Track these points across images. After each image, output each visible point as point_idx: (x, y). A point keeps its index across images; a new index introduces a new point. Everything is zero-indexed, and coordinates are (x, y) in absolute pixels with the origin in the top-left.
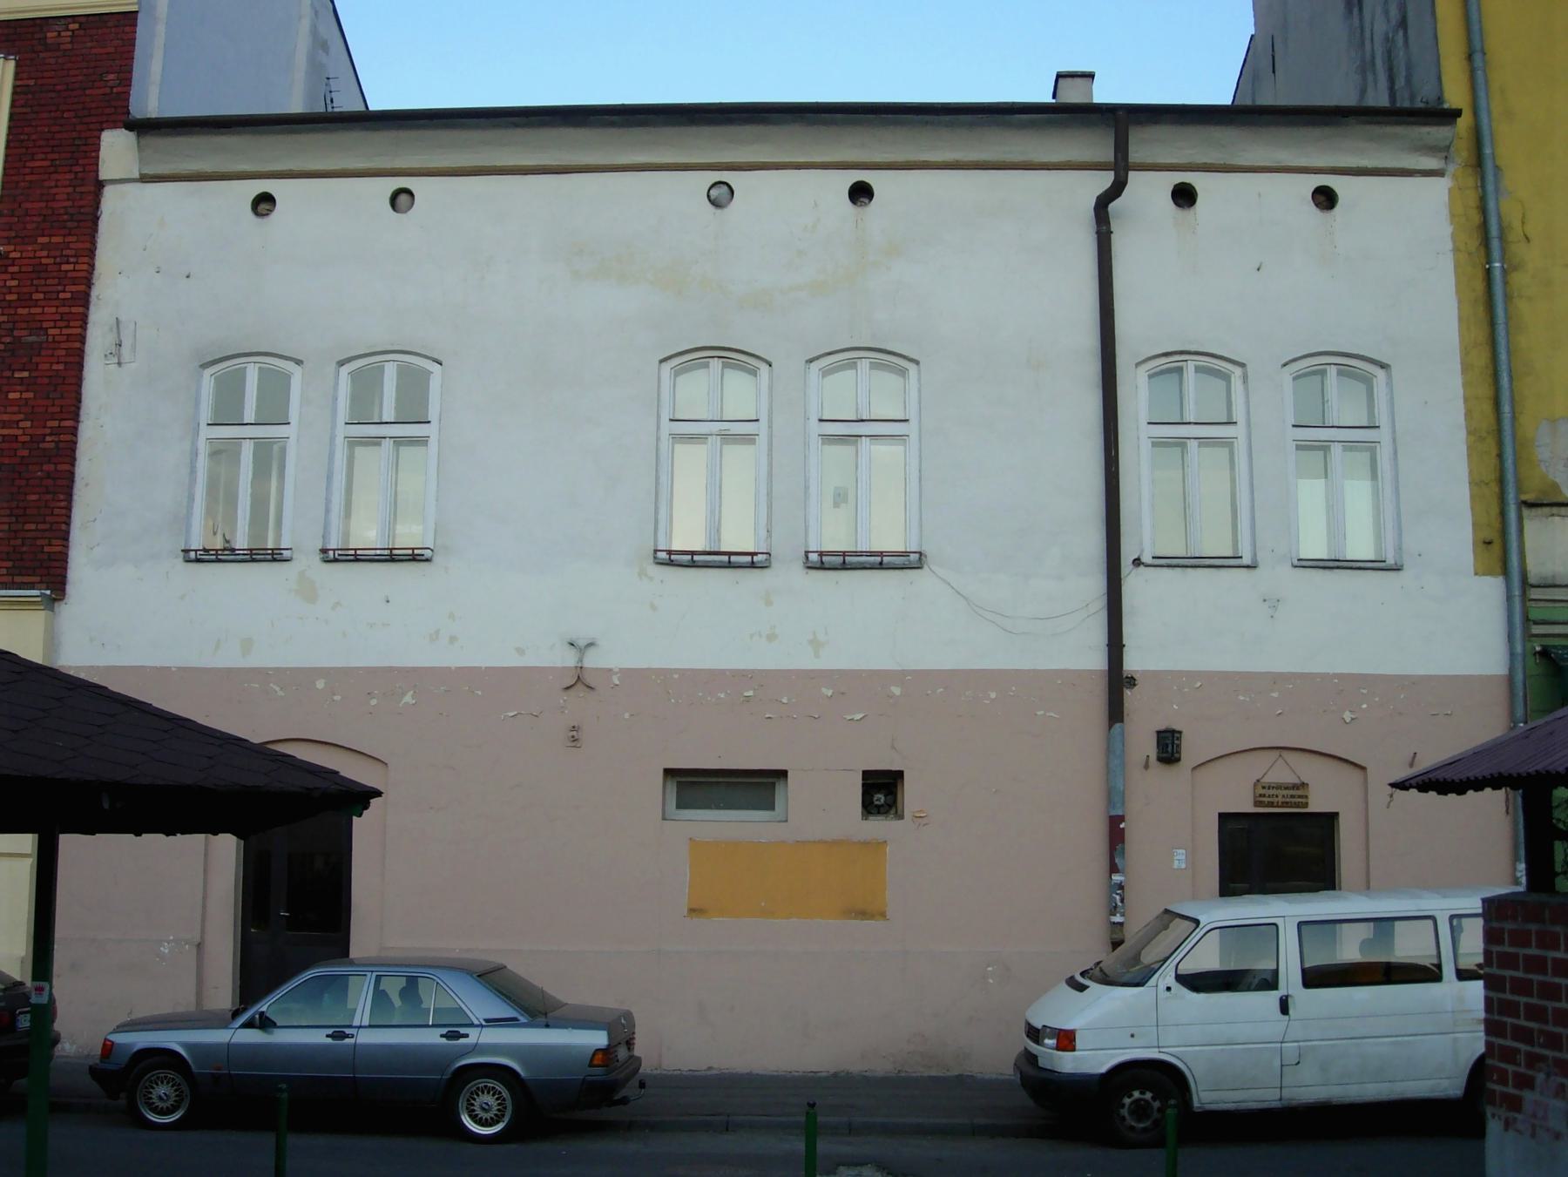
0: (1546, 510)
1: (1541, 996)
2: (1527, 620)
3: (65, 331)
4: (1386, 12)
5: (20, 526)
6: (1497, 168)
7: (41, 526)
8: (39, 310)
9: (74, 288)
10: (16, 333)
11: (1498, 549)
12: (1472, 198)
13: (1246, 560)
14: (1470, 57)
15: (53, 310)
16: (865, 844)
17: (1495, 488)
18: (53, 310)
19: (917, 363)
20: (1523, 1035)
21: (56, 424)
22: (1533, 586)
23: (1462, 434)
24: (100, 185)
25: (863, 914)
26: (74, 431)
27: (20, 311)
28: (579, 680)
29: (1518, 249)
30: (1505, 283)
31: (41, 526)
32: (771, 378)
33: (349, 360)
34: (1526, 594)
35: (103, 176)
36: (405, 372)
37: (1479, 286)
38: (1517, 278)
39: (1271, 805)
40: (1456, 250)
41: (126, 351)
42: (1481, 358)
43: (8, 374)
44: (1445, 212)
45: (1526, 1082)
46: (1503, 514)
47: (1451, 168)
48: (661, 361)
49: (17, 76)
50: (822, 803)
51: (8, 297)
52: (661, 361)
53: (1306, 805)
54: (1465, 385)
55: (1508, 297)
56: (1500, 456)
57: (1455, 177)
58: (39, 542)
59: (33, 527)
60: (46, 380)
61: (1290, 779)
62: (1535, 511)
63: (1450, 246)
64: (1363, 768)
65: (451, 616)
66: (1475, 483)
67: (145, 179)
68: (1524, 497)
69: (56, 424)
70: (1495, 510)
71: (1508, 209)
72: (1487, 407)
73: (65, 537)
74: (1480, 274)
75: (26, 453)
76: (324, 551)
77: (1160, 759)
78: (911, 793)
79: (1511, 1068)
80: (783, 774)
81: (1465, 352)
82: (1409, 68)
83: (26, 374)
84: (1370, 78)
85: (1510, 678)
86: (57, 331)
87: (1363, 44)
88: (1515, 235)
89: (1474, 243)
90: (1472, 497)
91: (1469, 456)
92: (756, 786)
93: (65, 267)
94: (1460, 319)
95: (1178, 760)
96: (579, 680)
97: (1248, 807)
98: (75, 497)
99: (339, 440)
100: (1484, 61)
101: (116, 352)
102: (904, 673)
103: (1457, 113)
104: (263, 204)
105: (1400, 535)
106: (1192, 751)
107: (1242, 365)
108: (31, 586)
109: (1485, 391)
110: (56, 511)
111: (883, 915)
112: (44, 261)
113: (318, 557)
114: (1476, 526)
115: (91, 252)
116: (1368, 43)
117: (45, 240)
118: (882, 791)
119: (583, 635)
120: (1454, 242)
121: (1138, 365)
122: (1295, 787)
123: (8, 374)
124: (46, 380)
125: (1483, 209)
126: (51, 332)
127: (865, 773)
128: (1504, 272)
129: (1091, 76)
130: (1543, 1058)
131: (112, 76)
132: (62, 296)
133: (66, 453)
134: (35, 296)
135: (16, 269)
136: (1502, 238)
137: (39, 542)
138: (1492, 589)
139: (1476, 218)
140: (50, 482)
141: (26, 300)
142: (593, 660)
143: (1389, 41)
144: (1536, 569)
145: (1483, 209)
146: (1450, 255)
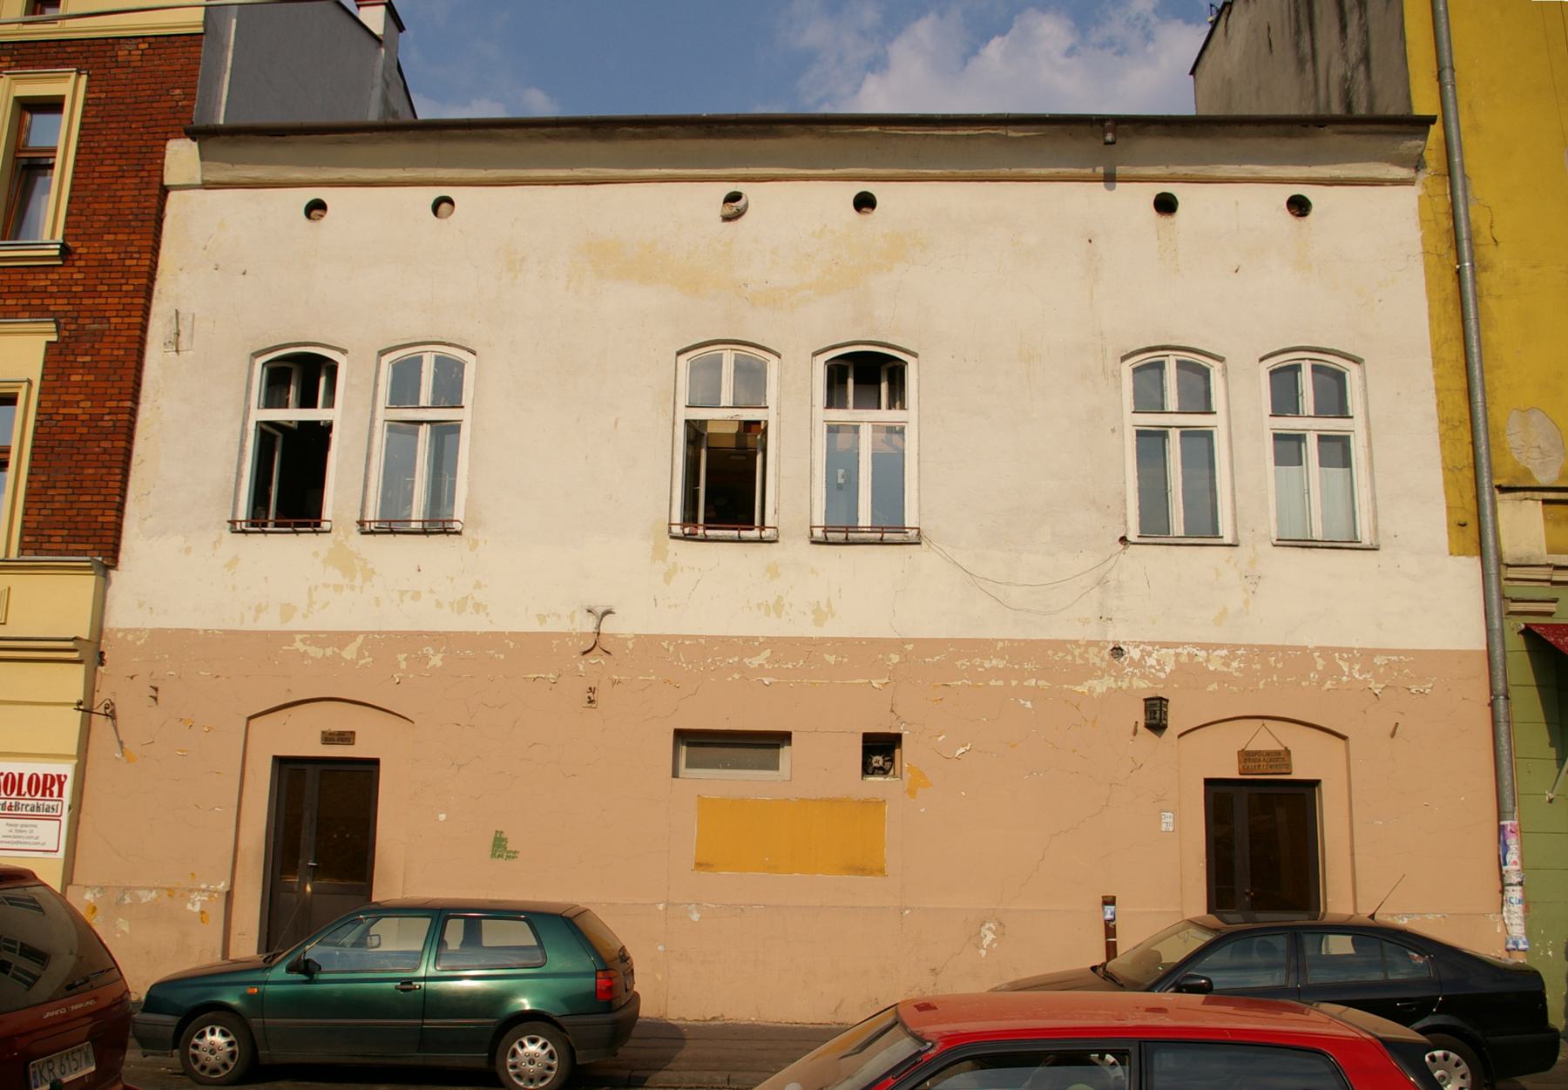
0: (1520, 494)
3: (127, 320)
4: (1345, 55)
5: (75, 498)
6: (1464, 176)
7: (96, 498)
9: (136, 282)
11: (1474, 531)
12: (1442, 204)
13: (1228, 539)
17: (1470, 474)
21: (114, 404)
22: (1509, 566)
23: (1435, 423)
24: (165, 191)
25: (862, 871)
27: (85, 301)
28: (595, 645)
29: (1488, 252)
30: (1475, 282)
31: (96, 498)
34: (1499, 574)
35: (166, 182)
36: (441, 361)
37: (1450, 285)
38: (1484, 278)
40: (1426, 253)
42: (1454, 352)
43: (71, 358)
46: (1478, 498)
48: (679, 353)
49: (89, 89)
50: (822, 763)
52: (679, 353)
54: (1437, 377)
56: (1474, 443)
57: (1425, 186)
58: (93, 512)
59: (88, 498)
60: (107, 365)
61: (1273, 746)
62: (1507, 496)
63: (1420, 249)
64: (1344, 738)
67: (206, 185)
69: (114, 404)
71: (1476, 215)
74: (1450, 276)
75: (85, 430)
76: (361, 523)
77: (1148, 726)
78: (906, 755)
80: (784, 738)
83: (88, 359)
88: (1485, 236)
89: (1444, 246)
90: (1446, 482)
91: (1442, 443)
93: (128, 262)
94: (1430, 316)
95: (1165, 727)
97: (1233, 774)
98: (132, 473)
99: (379, 423)
100: (1453, 77)
103: (1431, 120)
105: (1375, 516)
106: (1175, 722)
108: (85, 553)
110: (111, 484)
111: (882, 871)
113: (356, 528)
114: (1450, 509)
116: (1322, 92)
117: (111, 237)
120: (1424, 244)
123: (71, 358)
124: (107, 365)
126: (114, 320)
127: (865, 735)
132: (125, 288)
134: (100, 288)
135: (82, 263)
136: (1470, 240)
137: (93, 512)
138: (1470, 566)
139: (1447, 223)
141: (92, 292)
142: (608, 626)
144: (1510, 551)
146: (1420, 257)
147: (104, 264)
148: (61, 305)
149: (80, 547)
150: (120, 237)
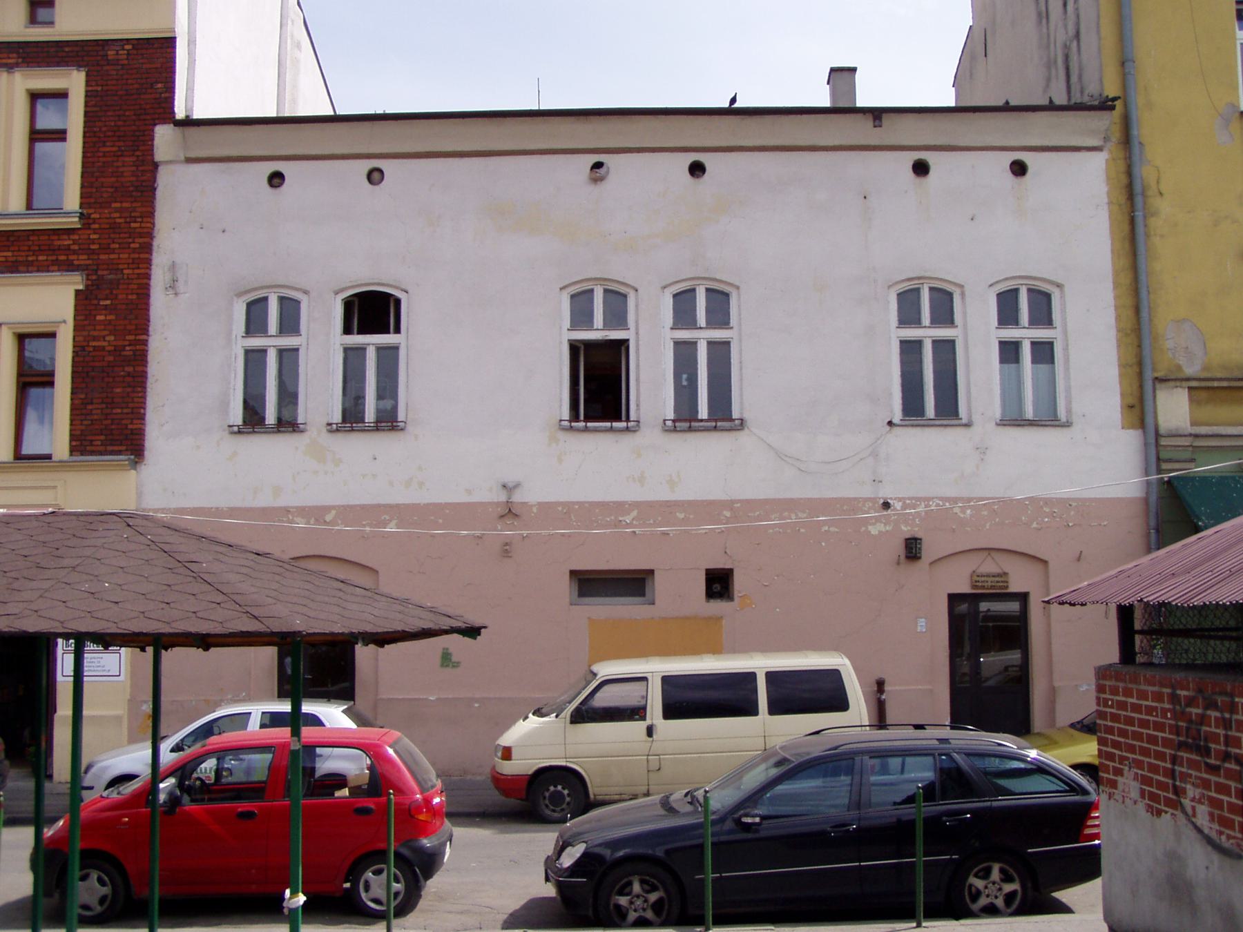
1: (1112, 720)
2: (1158, 459)
3: (137, 271)
4: (1066, 27)
5: (109, 411)
8: (115, 256)
9: (141, 240)
10: (100, 273)
11: (1138, 411)
12: (1122, 166)
13: (964, 421)
14: (1123, 64)
15: (126, 256)
16: (710, 618)
18: (126, 256)
19: (738, 288)
20: (1116, 745)
26: (145, 343)
27: (102, 257)
28: (510, 512)
32: (637, 299)
33: (342, 290)
38: (1153, 222)
39: (983, 587)
40: (1110, 203)
41: (181, 286)
42: (1126, 279)
44: (1103, 177)
45: (1118, 772)
46: (1141, 387)
47: (1109, 145)
50: (679, 590)
51: (93, 247)
53: (1007, 587)
54: (1116, 297)
55: (1147, 235)
62: (1163, 385)
63: (1106, 200)
64: (1045, 562)
65: (420, 468)
66: (1122, 366)
67: (189, 160)
68: (1156, 375)
70: (1136, 386)
71: (1145, 173)
72: (1130, 313)
73: (142, 418)
75: (111, 358)
79: (1111, 764)
81: (1116, 274)
82: (1081, 69)
83: (108, 302)
84: (1053, 72)
85: (1146, 500)
86: (130, 271)
87: (1048, 46)
89: (1123, 199)
91: (1119, 346)
92: (634, 583)
93: (133, 225)
94: (1112, 252)
96: (510, 512)
101: (173, 286)
102: (733, 502)
104: (276, 179)
106: (929, 551)
107: (961, 286)
109: (1129, 301)
112: (118, 220)
115: (150, 214)
116: (1052, 46)
117: (118, 205)
118: (719, 583)
119: (511, 479)
121: (889, 287)
122: (999, 575)
125: (1129, 173)
128: (1145, 217)
129: (854, 70)
130: (1127, 758)
131: (160, 85)
133: (141, 358)
135: (97, 226)
140: (130, 379)
141: (106, 249)
142: (517, 497)
143: (1066, 47)
145: (1129, 173)
146: (1106, 207)
147: (114, 227)
148: (83, 259)
149: (116, 448)
150: (125, 205)
